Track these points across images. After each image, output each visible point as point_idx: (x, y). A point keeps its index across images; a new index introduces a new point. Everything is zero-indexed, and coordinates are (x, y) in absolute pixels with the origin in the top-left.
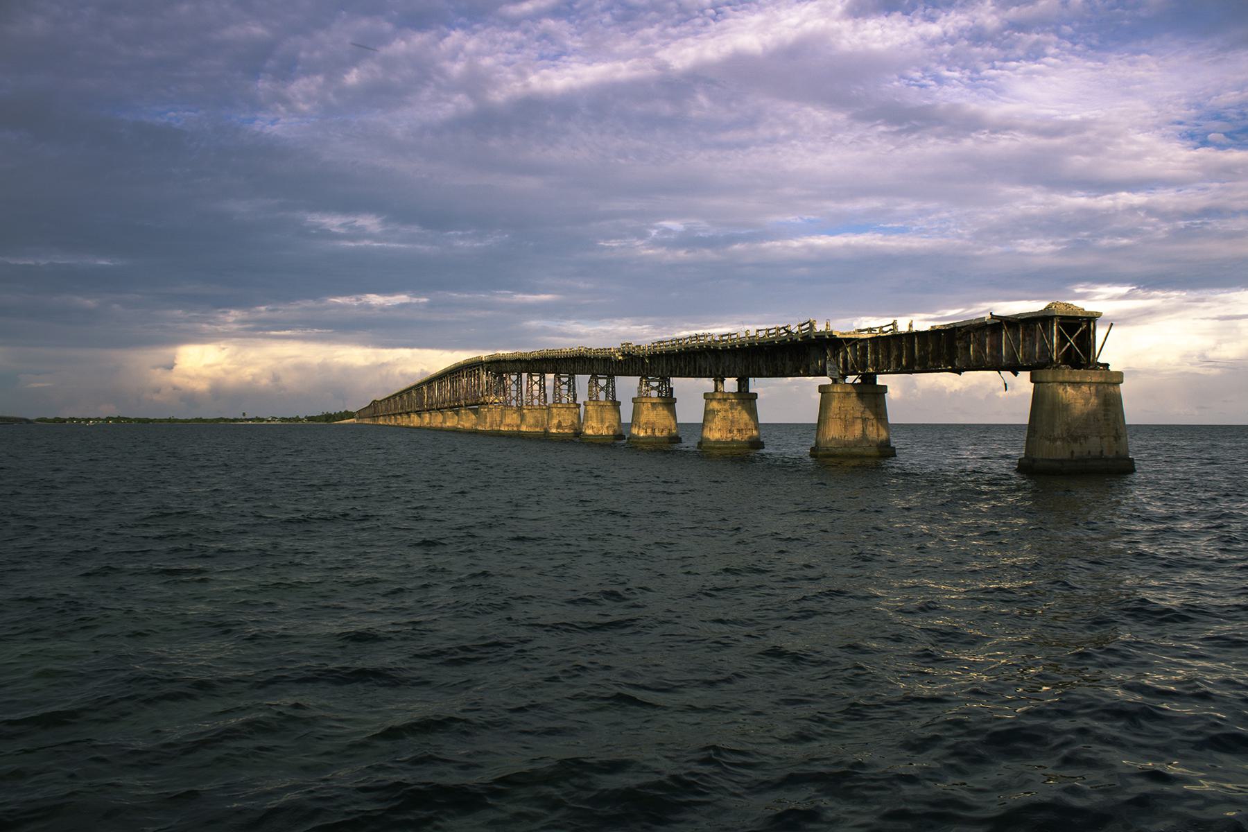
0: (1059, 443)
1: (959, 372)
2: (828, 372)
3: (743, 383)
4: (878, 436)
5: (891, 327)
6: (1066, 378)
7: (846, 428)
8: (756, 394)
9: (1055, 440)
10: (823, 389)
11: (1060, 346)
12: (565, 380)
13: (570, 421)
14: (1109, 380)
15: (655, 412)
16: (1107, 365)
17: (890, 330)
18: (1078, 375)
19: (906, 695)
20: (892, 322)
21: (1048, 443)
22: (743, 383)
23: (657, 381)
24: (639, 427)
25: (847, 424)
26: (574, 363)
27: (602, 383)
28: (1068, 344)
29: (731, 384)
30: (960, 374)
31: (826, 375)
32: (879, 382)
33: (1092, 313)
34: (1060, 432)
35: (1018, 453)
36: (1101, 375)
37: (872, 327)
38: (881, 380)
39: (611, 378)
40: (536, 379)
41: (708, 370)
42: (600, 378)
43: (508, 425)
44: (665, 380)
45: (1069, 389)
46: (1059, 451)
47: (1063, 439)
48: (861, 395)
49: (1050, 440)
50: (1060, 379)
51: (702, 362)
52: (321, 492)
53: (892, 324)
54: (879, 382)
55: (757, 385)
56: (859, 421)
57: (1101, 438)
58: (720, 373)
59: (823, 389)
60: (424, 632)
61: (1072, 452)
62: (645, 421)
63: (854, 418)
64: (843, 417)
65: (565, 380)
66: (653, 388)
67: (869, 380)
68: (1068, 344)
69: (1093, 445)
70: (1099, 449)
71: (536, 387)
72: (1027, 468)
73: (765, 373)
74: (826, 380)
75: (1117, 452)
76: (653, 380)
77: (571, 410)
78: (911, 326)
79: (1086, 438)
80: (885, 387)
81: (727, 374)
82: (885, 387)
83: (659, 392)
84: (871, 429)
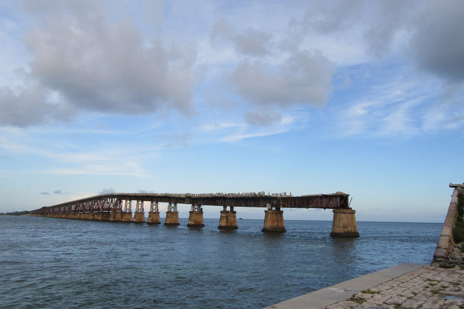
0: (341, 228)
1: (307, 208)
2: (267, 207)
3: (232, 208)
4: (281, 225)
5: (284, 194)
6: (342, 211)
7: (273, 223)
8: (236, 212)
9: (340, 228)
10: (265, 211)
11: (340, 203)
12: (155, 204)
13: (156, 218)
14: (352, 212)
15: (197, 216)
16: (351, 208)
17: (284, 195)
18: (345, 210)
19: (425, 294)
20: (284, 192)
21: (338, 228)
22: (232, 208)
23: (197, 206)
24: (192, 221)
25: (273, 222)
26: (172, 199)
27: (173, 205)
28: (342, 203)
29: (228, 208)
30: (325, 209)
31: (266, 207)
32: (281, 210)
33: (347, 195)
34: (341, 226)
35: (262, 225)
36: (351, 211)
37: (278, 193)
38: (282, 209)
39: (175, 204)
40: (128, 202)
41: (221, 203)
42: (172, 204)
43: (125, 219)
44: (200, 206)
45: (343, 214)
46: (341, 230)
47: (342, 227)
48: (276, 214)
49: (339, 228)
50: (341, 212)
51: (218, 201)
52: (298, 261)
53: (285, 193)
54: (281, 210)
55: (236, 209)
56: (276, 221)
57: (351, 227)
58: (226, 205)
59: (265, 211)
60: (237, 294)
61: (345, 231)
62: (193, 219)
63: (275, 220)
64: (272, 220)
65: (155, 204)
66: (196, 208)
67: (278, 209)
68: (342, 203)
69: (350, 229)
70: (351, 230)
71: (140, 206)
72: (264, 230)
73: (243, 206)
74: (266, 209)
75: (355, 231)
76: (196, 206)
77: (157, 214)
78: (291, 194)
79: (347, 227)
80: (283, 211)
81: (228, 205)
82: (283, 211)
83: (198, 209)
84: (279, 223)
